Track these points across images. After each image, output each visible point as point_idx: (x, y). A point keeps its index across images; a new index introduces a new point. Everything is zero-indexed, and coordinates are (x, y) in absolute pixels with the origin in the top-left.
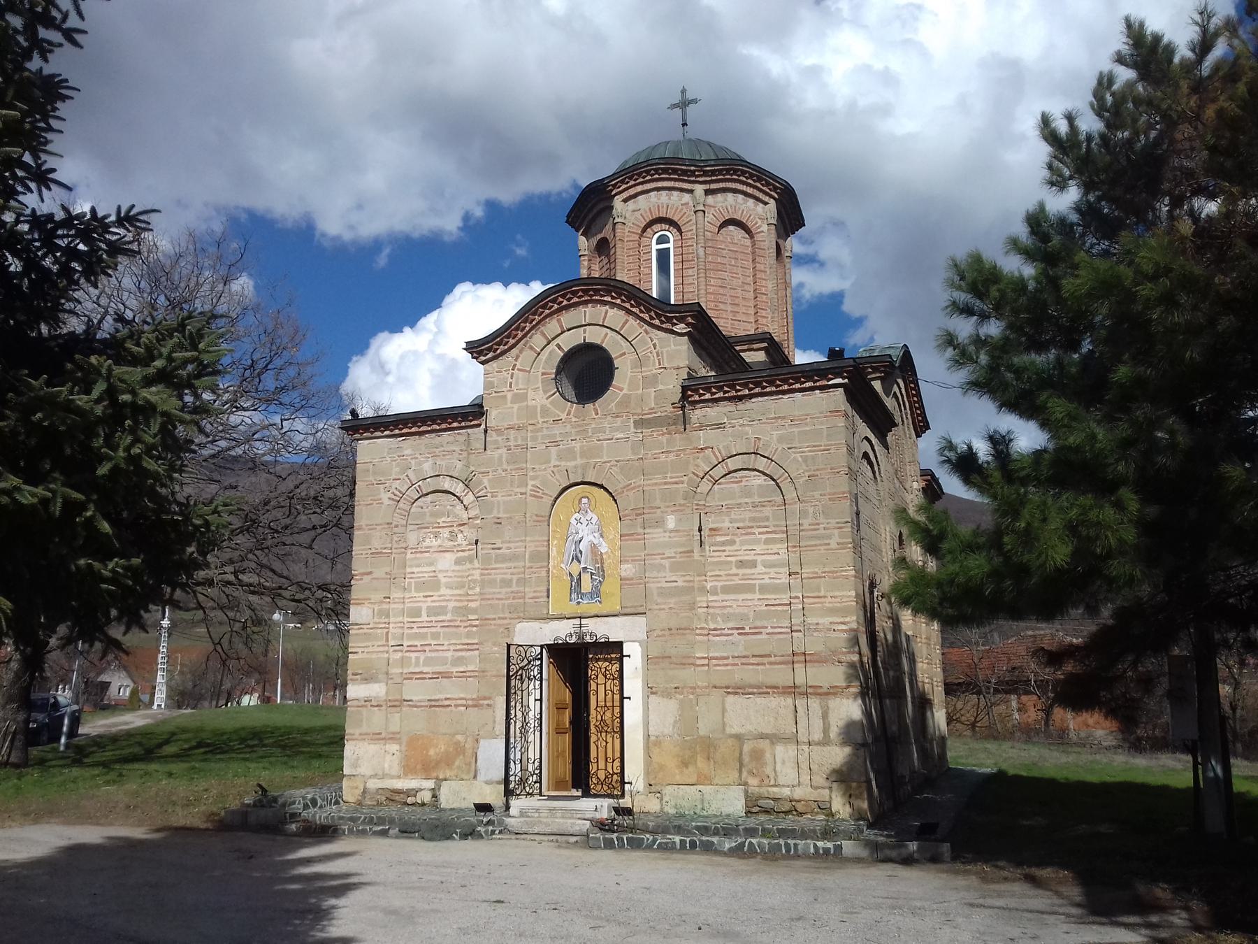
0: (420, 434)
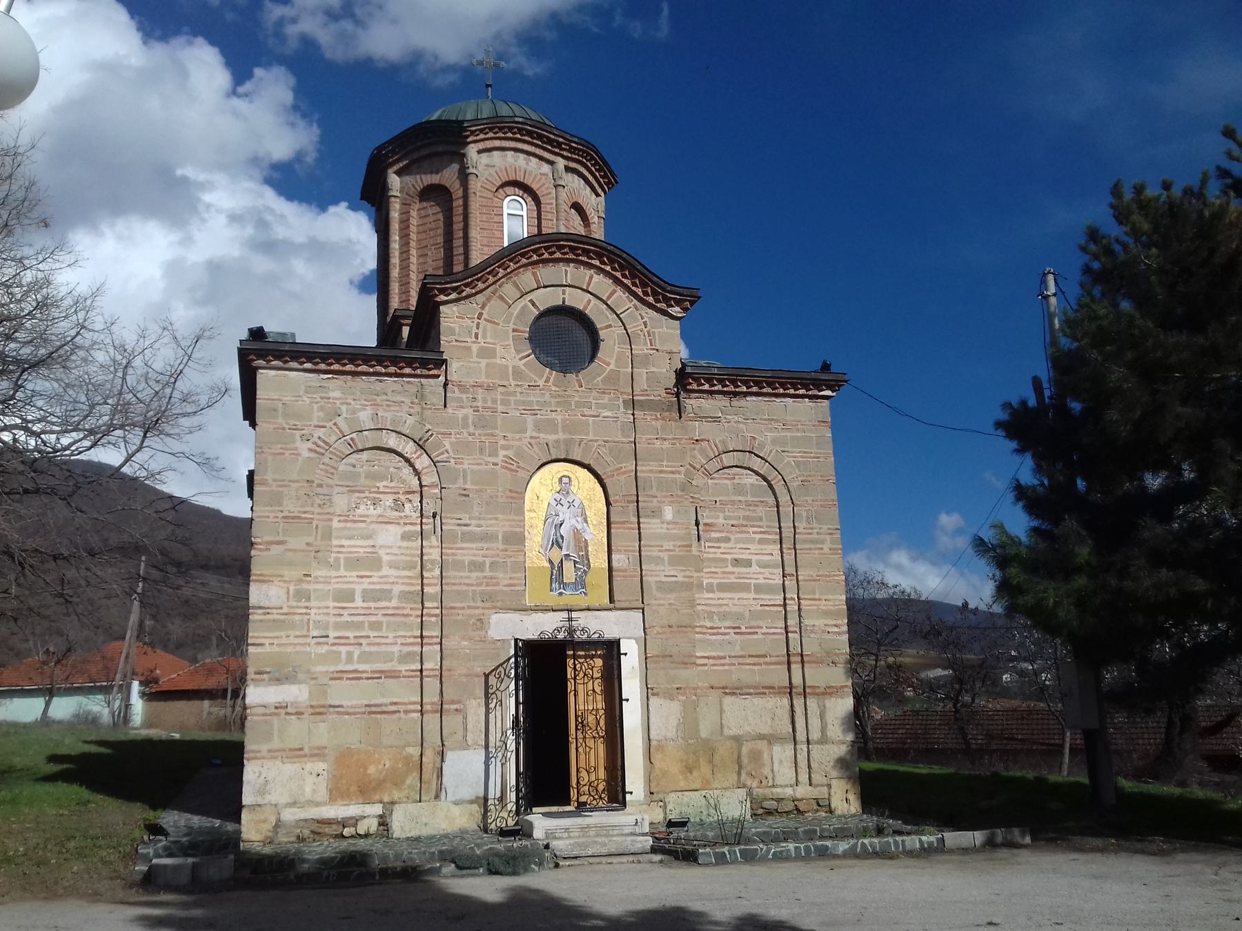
0: (354, 374)
